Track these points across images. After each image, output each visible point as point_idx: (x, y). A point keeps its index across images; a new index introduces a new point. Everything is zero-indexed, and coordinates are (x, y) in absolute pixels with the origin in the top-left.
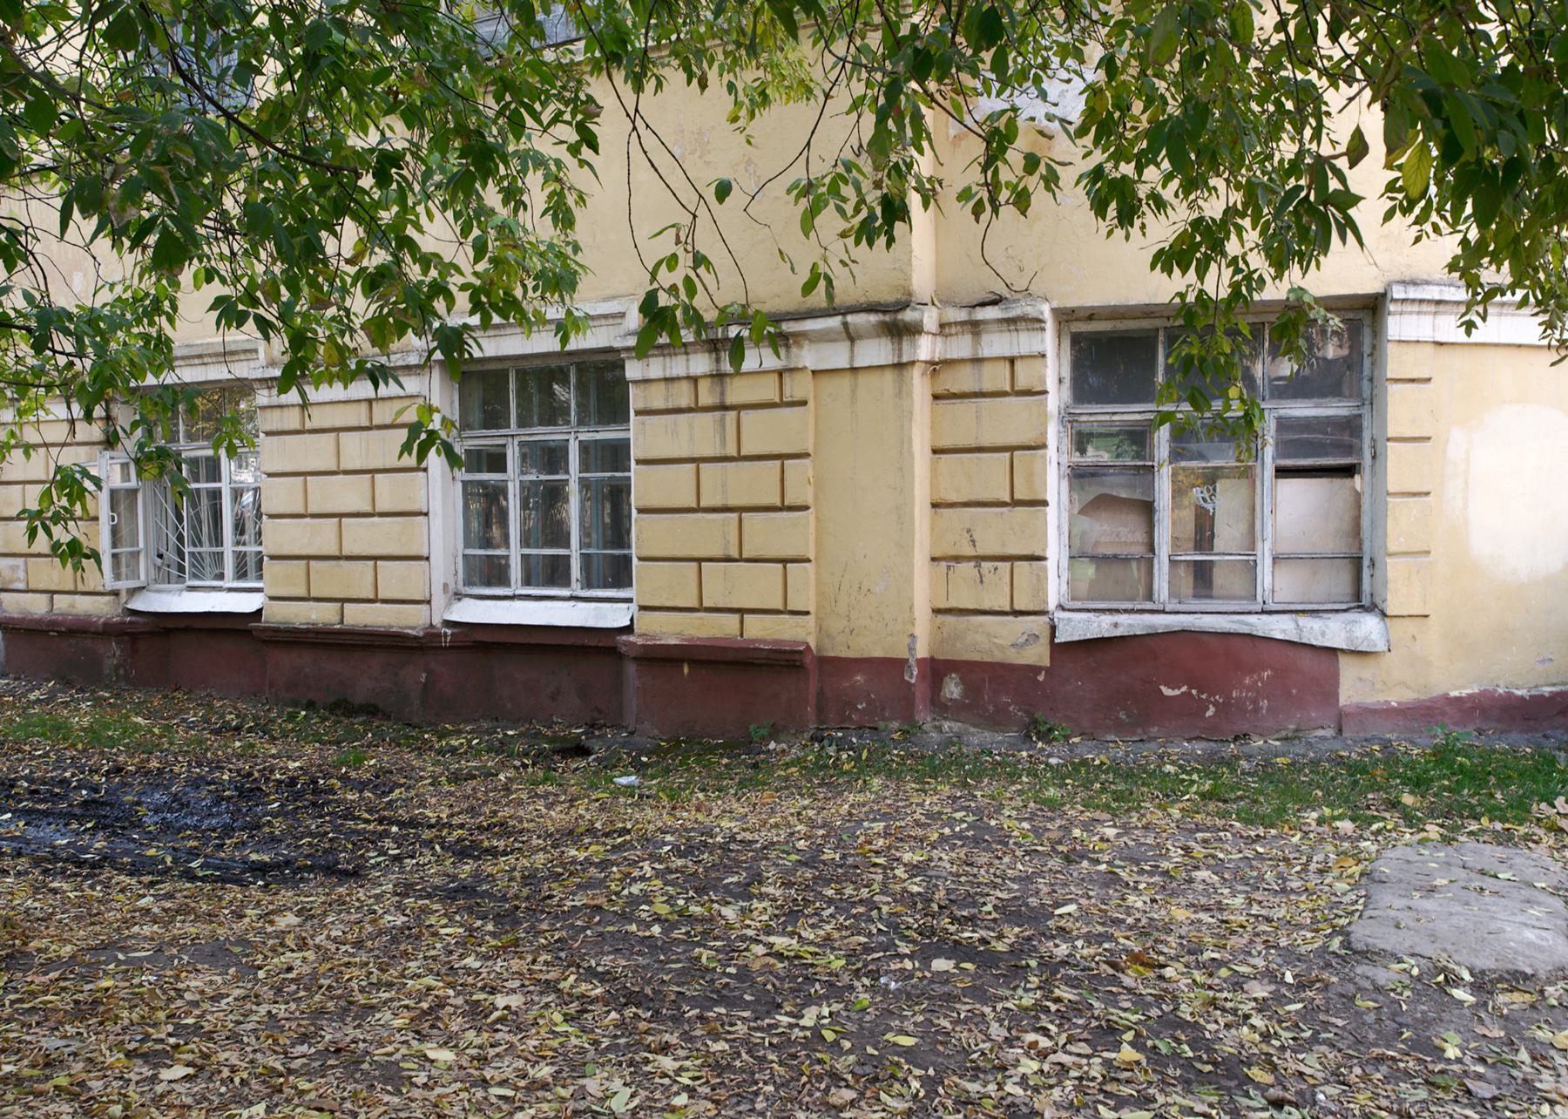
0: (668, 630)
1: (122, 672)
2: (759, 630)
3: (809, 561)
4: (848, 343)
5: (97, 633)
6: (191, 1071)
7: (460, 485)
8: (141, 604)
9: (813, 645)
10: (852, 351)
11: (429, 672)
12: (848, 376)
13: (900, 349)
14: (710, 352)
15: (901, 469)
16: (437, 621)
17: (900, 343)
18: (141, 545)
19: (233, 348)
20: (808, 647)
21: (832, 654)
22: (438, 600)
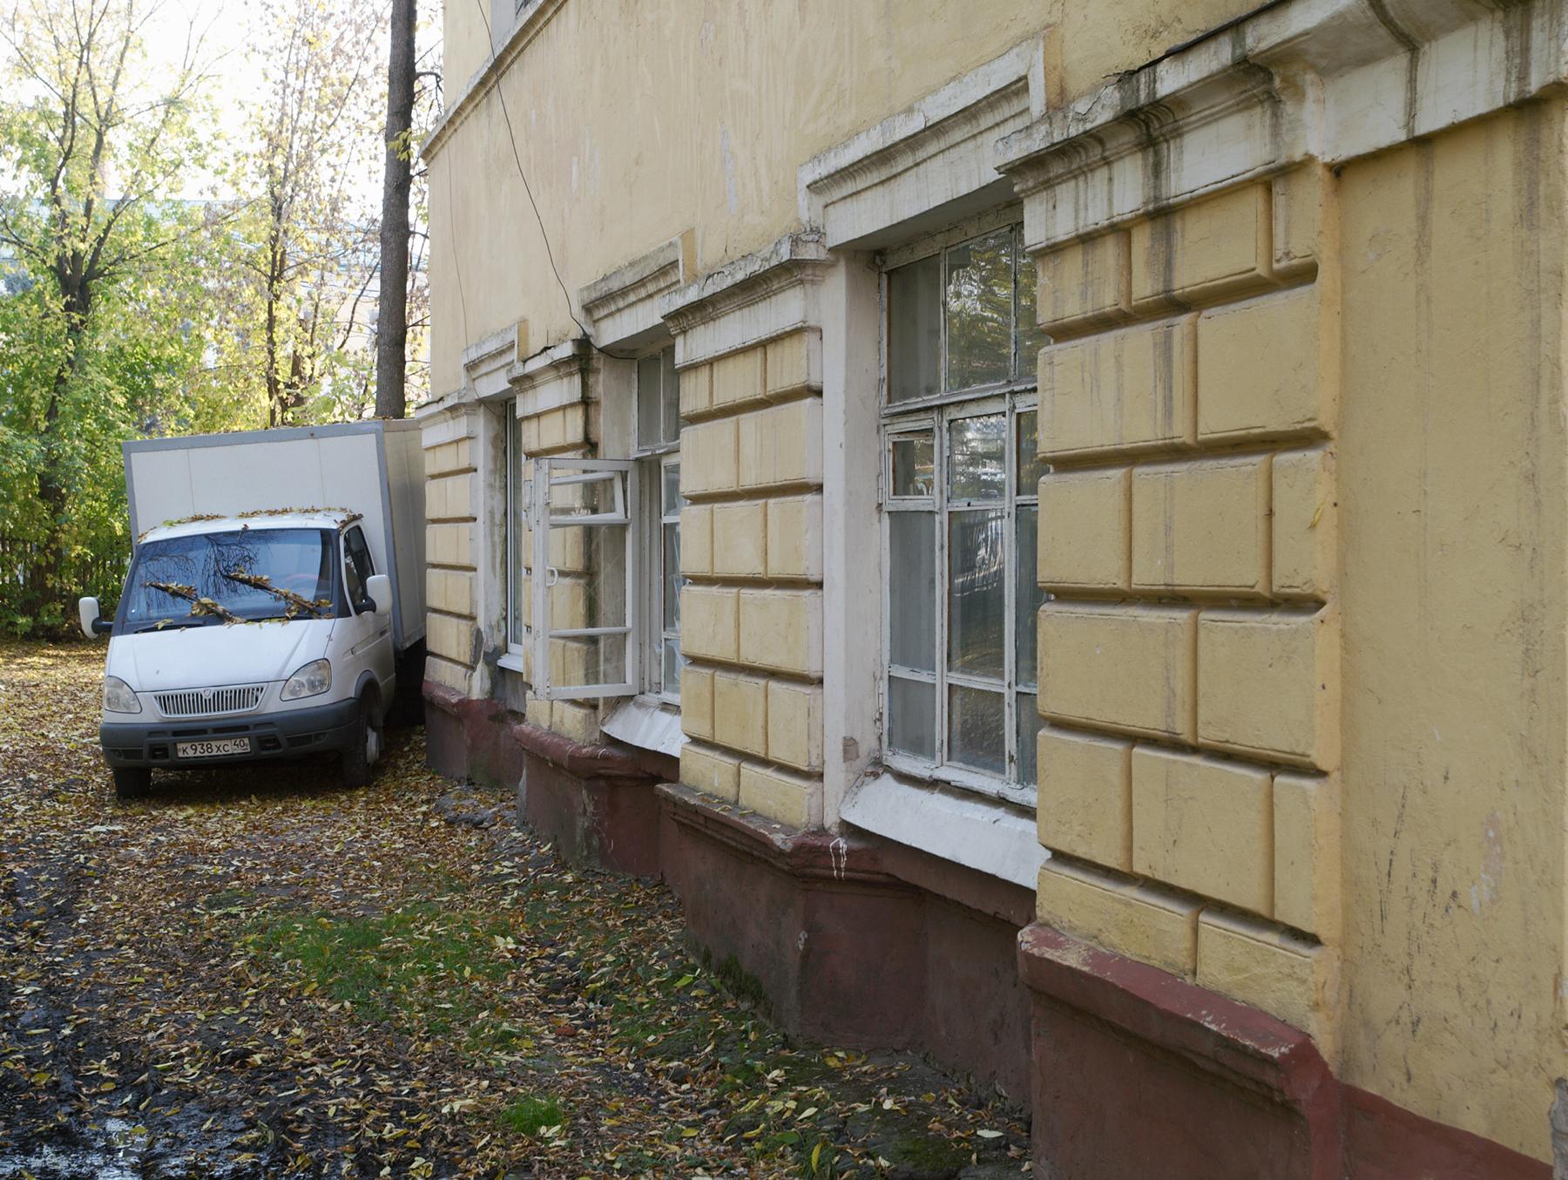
0: (1081, 924)
1: (595, 842)
2: (1231, 964)
3: (1320, 774)
4: (1402, 60)
5: (558, 766)
6: (103, 114)
7: (886, 519)
8: (618, 728)
9: (1325, 1045)
10: (1412, 82)
11: (811, 927)
12: (1410, 163)
13: (1525, 50)
14: (1245, 105)
15: (1531, 478)
16: (830, 821)
17: (1525, 30)
18: (629, 624)
19: (591, 380)
20: (1305, 1051)
21: (1373, 1089)
22: (836, 772)
